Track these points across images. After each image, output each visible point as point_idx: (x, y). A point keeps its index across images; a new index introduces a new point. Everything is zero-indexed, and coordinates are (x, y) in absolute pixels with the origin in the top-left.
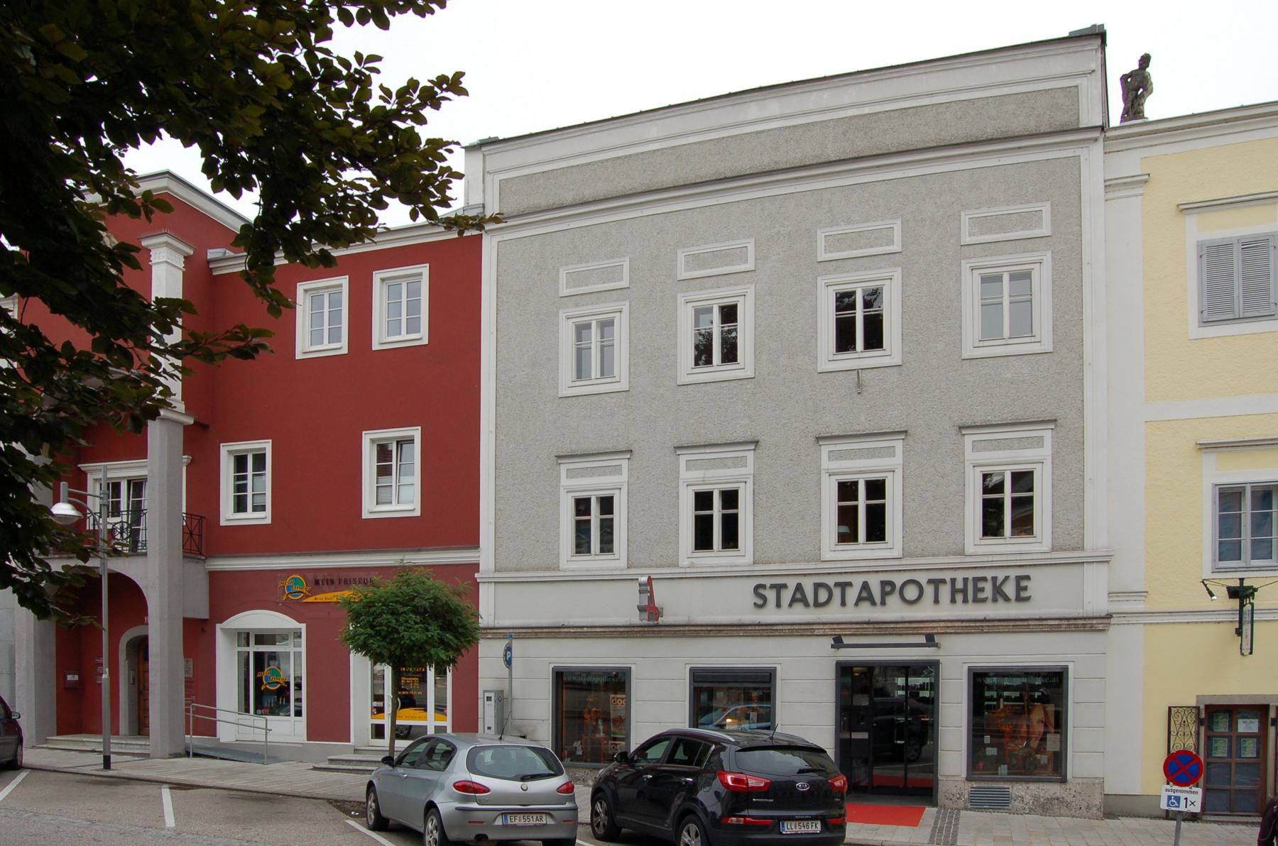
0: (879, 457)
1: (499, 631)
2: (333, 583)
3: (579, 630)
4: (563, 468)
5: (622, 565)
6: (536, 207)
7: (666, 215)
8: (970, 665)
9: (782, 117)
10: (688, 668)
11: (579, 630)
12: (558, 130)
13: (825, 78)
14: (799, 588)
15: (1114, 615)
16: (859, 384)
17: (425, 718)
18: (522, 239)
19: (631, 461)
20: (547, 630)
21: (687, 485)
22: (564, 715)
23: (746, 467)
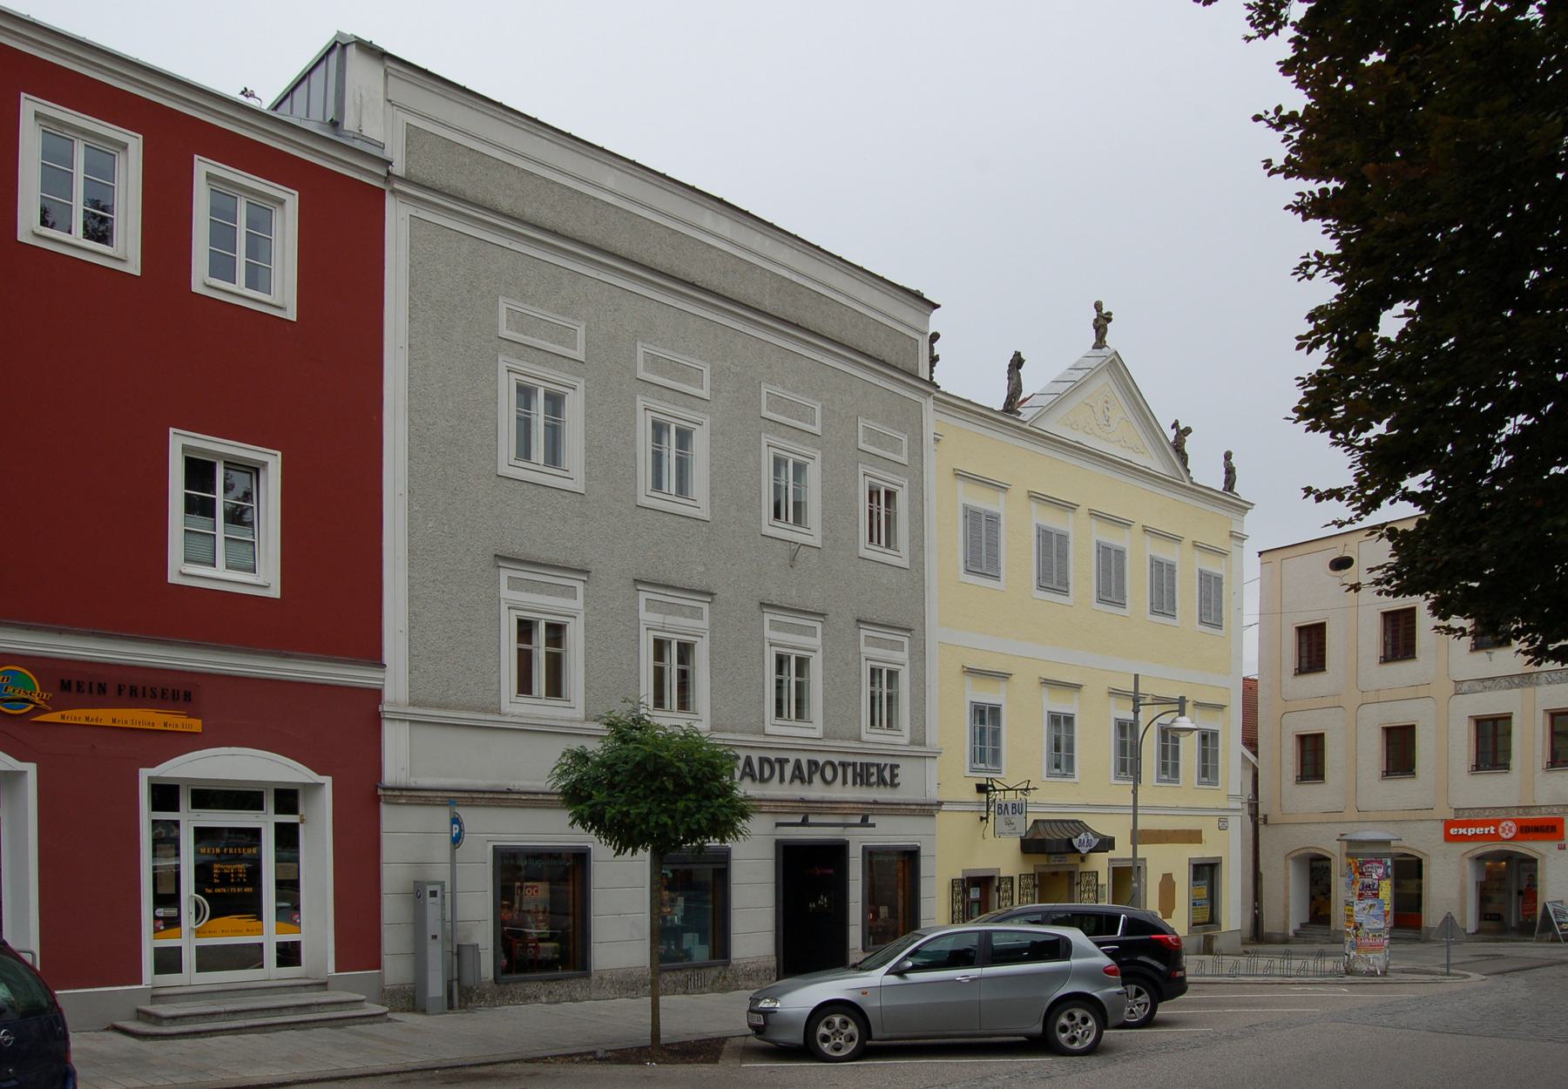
1: (421, 794)
2: (104, 692)
3: (532, 797)
5: (578, 716)
7: (624, 292)
9: (731, 242)
10: (490, 848)
11: (532, 797)
12: (500, 105)
13: (464, 89)
14: (798, 764)
17: (260, 932)
19: (712, 605)
20: (491, 796)
22: (710, 906)
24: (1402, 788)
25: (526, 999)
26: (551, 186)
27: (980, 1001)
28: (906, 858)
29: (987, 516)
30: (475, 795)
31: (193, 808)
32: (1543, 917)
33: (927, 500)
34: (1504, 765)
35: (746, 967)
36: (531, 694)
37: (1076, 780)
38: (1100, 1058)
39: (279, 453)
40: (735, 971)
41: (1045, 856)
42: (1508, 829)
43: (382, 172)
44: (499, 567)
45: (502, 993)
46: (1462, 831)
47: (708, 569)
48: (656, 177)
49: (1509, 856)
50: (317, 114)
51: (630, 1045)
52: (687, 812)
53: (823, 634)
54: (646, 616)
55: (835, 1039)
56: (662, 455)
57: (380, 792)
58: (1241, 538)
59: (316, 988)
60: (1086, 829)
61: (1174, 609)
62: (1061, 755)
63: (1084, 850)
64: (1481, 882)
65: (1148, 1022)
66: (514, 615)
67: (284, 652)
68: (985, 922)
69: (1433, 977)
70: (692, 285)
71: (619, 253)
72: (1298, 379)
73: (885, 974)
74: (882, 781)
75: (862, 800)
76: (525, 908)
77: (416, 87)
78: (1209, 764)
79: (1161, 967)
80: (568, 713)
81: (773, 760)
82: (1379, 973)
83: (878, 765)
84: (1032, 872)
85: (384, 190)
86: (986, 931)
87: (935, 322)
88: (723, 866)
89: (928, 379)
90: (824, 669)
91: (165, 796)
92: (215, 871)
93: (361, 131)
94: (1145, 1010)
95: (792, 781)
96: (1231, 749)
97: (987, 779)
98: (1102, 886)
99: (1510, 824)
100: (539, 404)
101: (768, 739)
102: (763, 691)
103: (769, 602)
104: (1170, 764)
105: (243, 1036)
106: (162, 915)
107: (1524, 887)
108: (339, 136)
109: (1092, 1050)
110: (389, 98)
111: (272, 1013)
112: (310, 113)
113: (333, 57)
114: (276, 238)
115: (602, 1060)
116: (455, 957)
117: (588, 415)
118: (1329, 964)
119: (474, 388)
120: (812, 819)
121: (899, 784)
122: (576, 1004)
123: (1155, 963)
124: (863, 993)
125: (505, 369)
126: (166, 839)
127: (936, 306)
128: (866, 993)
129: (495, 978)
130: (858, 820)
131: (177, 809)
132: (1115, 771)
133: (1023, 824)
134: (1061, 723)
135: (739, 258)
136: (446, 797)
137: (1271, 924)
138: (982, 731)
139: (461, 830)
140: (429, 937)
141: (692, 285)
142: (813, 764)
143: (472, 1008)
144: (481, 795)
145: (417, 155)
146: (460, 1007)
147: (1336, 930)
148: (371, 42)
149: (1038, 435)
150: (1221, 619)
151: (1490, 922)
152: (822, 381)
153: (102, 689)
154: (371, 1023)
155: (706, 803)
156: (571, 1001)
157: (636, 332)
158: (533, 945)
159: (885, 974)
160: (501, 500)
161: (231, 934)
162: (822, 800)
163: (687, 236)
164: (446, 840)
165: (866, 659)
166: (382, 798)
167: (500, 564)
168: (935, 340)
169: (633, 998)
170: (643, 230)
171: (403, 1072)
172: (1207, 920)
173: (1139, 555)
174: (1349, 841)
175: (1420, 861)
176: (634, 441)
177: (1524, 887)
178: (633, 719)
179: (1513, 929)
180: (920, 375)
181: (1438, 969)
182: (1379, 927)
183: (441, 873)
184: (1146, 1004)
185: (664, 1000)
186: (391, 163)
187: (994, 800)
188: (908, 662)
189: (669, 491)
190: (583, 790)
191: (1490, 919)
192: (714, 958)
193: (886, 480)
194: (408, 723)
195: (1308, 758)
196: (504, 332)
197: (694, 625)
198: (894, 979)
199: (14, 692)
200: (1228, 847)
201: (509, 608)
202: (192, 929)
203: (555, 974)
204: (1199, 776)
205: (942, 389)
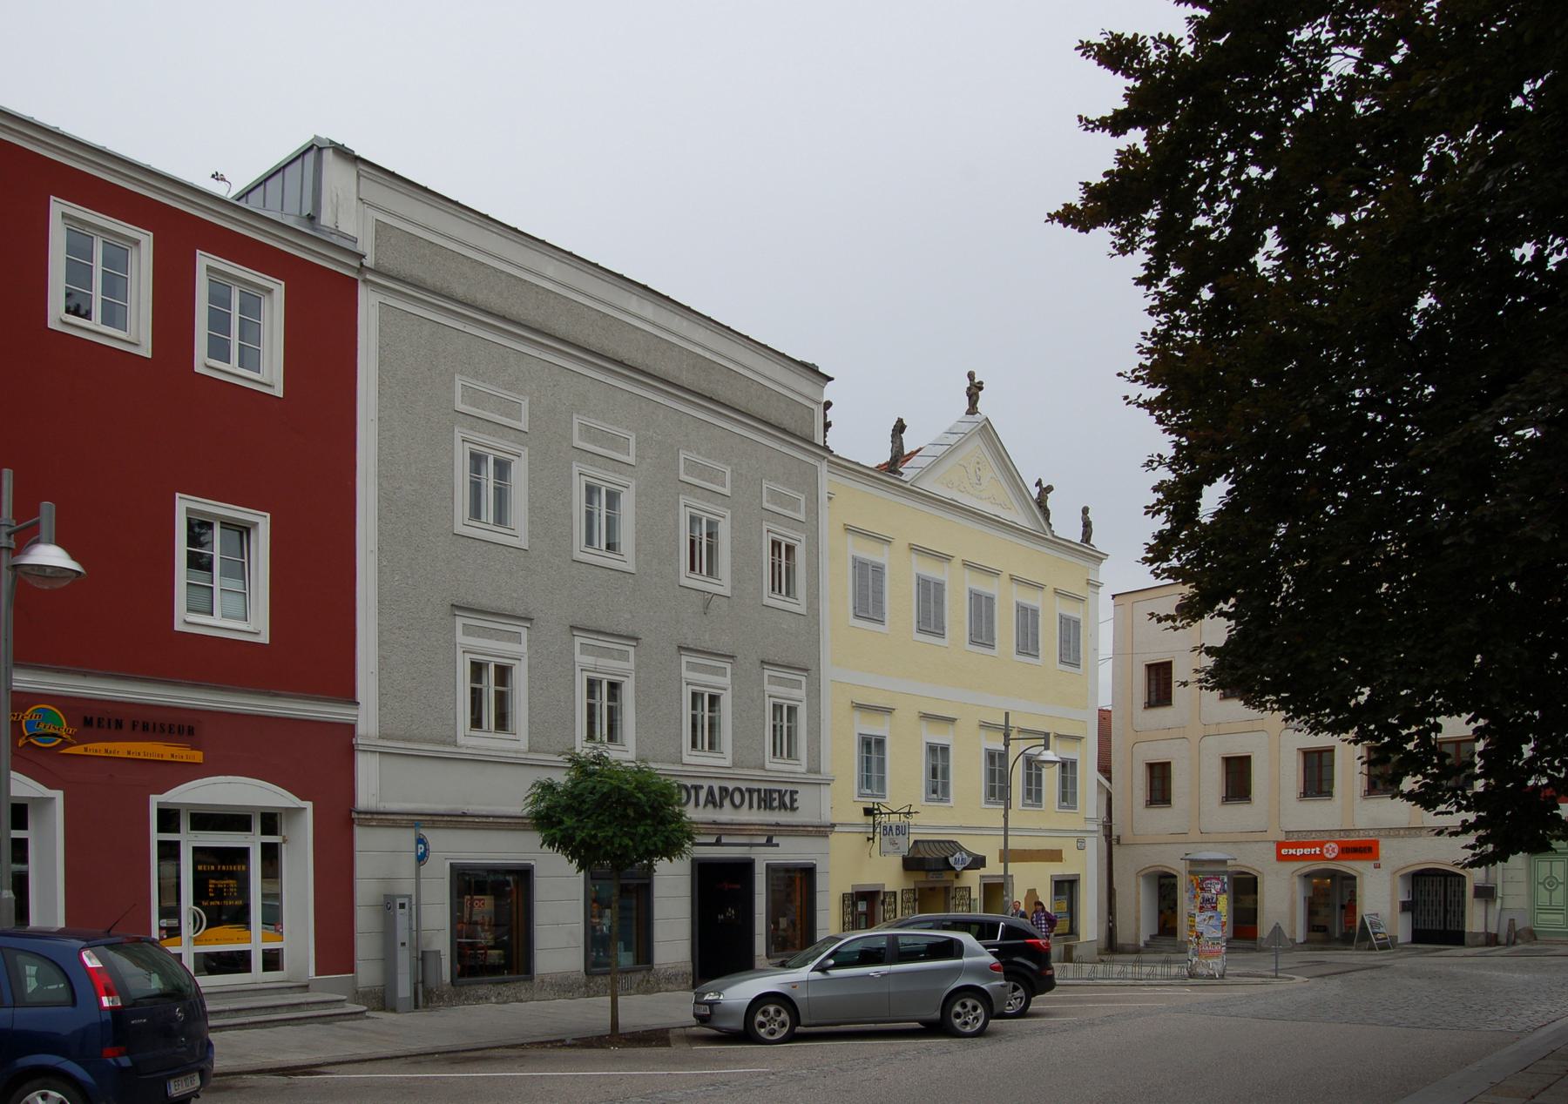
2: (121, 727)
3: (484, 820)
6: (421, 282)
8: (452, 861)
9: (653, 324)
10: (448, 866)
11: (484, 820)
12: (456, 203)
13: (425, 189)
14: (711, 789)
17: (249, 940)
18: (409, 315)
20: (449, 819)
21: (464, 652)
22: (634, 914)
24: (1238, 813)
25: (479, 999)
26: (498, 274)
27: (889, 993)
28: (804, 874)
29: (873, 567)
30: (436, 818)
31: (191, 830)
32: (1361, 928)
33: (822, 552)
34: (1329, 792)
36: (481, 728)
37: (951, 804)
38: (988, 1039)
42: (1332, 850)
43: (356, 264)
44: (455, 615)
46: (1292, 851)
47: (633, 617)
48: (589, 266)
49: (1333, 874)
50: (292, 206)
52: (645, 836)
53: (732, 674)
54: (581, 659)
57: (354, 815)
58: (1097, 586)
59: (300, 989)
60: (961, 849)
61: (1038, 650)
62: (938, 780)
63: (959, 868)
64: (1309, 898)
65: (1022, 1013)
67: (272, 691)
69: (1264, 979)
72: (1145, 544)
73: (811, 971)
74: (783, 806)
75: (766, 823)
76: (475, 918)
78: (1069, 790)
79: (1034, 967)
80: (514, 745)
82: (1217, 976)
83: (779, 791)
84: (913, 887)
85: (357, 280)
86: (893, 935)
87: (829, 392)
88: (647, 881)
89: (822, 445)
90: (733, 706)
91: (169, 819)
92: (210, 886)
94: (1020, 1003)
96: (1088, 775)
97: (874, 803)
98: (974, 900)
99: (1333, 845)
101: (685, 768)
103: (685, 646)
104: (1034, 791)
106: (165, 925)
107: (1346, 902)
109: (980, 1033)
110: (361, 197)
112: (285, 207)
113: (310, 157)
115: (570, 1046)
116: (420, 962)
118: (1175, 970)
120: (724, 840)
121: (798, 808)
123: (1029, 963)
126: (170, 852)
127: (830, 379)
129: (452, 981)
130: (763, 840)
131: (178, 831)
132: (986, 797)
133: (905, 845)
134: (938, 753)
135: (661, 338)
137: (1123, 937)
138: (868, 760)
139: (426, 850)
142: (723, 790)
143: (434, 1007)
144: (440, 818)
146: (424, 1007)
147: (1182, 941)
148: (343, 145)
149: (919, 493)
150: (1079, 659)
151: (1319, 934)
152: (732, 447)
153: (119, 724)
155: (660, 827)
156: (516, 1001)
157: (573, 405)
158: (482, 951)
159: (811, 971)
160: (457, 555)
161: (224, 942)
162: (731, 822)
165: (770, 696)
166: (356, 821)
167: (457, 613)
168: (828, 408)
171: (410, 1056)
172: (1067, 931)
173: (1006, 601)
174: (1192, 861)
175: (1256, 878)
176: (570, 503)
177: (1346, 902)
179: (1337, 939)
180: (816, 442)
181: (1269, 973)
182: (1217, 936)
183: (407, 887)
184: (1021, 998)
186: (364, 257)
187: (880, 822)
188: (526, 656)
190: (554, 816)
191: (1317, 931)
193: (787, 535)
194: (378, 754)
195: (1157, 783)
196: (460, 406)
197: (622, 666)
198: (818, 975)
199: (45, 727)
200: (1085, 864)
201: (464, 652)
202: (191, 937)
203: (501, 977)
204: (927, 793)
205: (835, 453)
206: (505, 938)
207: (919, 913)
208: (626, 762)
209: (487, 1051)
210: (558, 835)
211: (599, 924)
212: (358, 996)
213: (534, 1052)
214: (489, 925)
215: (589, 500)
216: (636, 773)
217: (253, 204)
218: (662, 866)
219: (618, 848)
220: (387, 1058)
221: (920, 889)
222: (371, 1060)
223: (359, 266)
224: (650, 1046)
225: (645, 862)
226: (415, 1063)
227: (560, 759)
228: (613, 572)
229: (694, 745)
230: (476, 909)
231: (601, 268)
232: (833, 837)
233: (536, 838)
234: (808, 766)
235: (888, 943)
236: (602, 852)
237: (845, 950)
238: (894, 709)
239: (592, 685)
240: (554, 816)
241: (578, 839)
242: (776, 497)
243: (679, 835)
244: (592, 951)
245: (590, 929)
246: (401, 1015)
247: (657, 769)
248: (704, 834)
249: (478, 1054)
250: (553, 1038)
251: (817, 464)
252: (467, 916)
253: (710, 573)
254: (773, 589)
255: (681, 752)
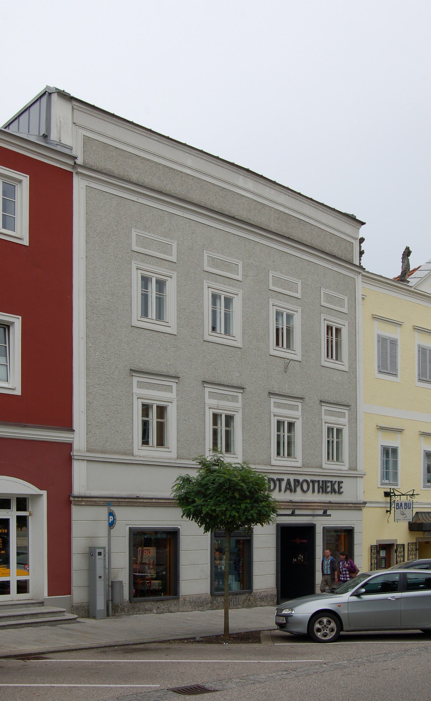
0: (292, 410)
1: (93, 499)
3: (150, 501)
4: (207, 390)
9: (253, 193)
10: (127, 529)
11: (150, 501)
12: (132, 123)
13: (113, 115)
14: (289, 482)
15: (367, 503)
16: (286, 368)
19: (244, 394)
20: (128, 500)
23: (238, 402)
25: (146, 611)
26: (158, 166)
28: (346, 534)
35: (260, 594)
36: (148, 445)
39: (20, 317)
40: (255, 596)
41: (422, 532)
43: (72, 163)
44: (133, 376)
45: (133, 608)
50: (34, 130)
51: (211, 634)
53: (302, 409)
54: (209, 401)
55: (324, 630)
56: (148, 296)
57: (72, 499)
66: (140, 401)
68: (404, 568)
70: (233, 218)
71: (194, 202)
73: (351, 596)
74: (333, 491)
75: (322, 501)
76: (144, 561)
77: (107, 123)
80: (168, 455)
81: (275, 479)
83: (331, 482)
85: (72, 173)
86: (403, 573)
87: (363, 232)
88: (249, 538)
89: (359, 265)
93: (60, 140)
95: (285, 491)
97: (390, 489)
100: (153, 286)
101: (273, 468)
102: (270, 441)
105: (6, 630)
108: (48, 143)
110: (74, 122)
111: (19, 618)
113: (44, 99)
114: (18, 200)
115: (199, 642)
116: (110, 588)
117: (178, 292)
119: (119, 279)
120: (297, 512)
121: (343, 492)
122: (172, 614)
124: (339, 606)
125: (135, 268)
127: (363, 224)
128: (340, 606)
129: (130, 599)
130: (321, 512)
133: (410, 515)
135: (257, 201)
136: (104, 501)
138: (387, 462)
139: (114, 519)
140: (98, 577)
141: (233, 218)
142: (297, 481)
143: (119, 616)
144: (123, 500)
145: (89, 153)
146: (113, 616)
148: (64, 91)
149: (419, 294)
154: (69, 623)
155: (255, 505)
156: (169, 612)
159: (351, 596)
160: (133, 339)
162: (301, 501)
163: (230, 191)
164: (105, 525)
166: (73, 502)
169: (202, 611)
170: (207, 189)
171: (100, 647)
178: (215, 460)
180: (354, 263)
183: (102, 542)
185: (231, 612)
186: (76, 158)
187: (394, 501)
188: (175, 400)
189: (152, 318)
192: (243, 589)
194: (86, 461)
198: (355, 598)
201: (138, 398)
204: (424, 482)
206: (164, 573)
207: (419, 558)
208: (235, 464)
209: (147, 644)
210: (192, 510)
211: (220, 564)
212: (74, 609)
213: (175, 646)
214: (153, 565)
215: (214, 303)
216: (240, 471)
217: (12, 130)
218: (257, 529)
219: (229, 518)
220: (85, 649)
221: (419, 542)
222: (76, 650)
223: (74, 165)
224: (248, 643)
225: (246, 526)
226: (102, 652)
227: (194, 462)
228: (228, 348)
229: (278, 454)
230: (145, 555)
231: (221, 159)
232: (364, 510)
233: (179, 511)
234: (349, 466)
235: (400, 578)
236: (219, 520)
237: (372, 582)
238: (404, 430)
239: (216, 417)
240: (190, 498)
241: (204, 512)
242: (330, 299)
243: (267, 509)
244: (215, 581)
245: (214, 567)
246: (99, 620)
247: (253, 469)
248: (283, 509)
249: (142, 646)
250: (188, 637)
251: (355, 277)
252: (139, 560)
253: (288, 347)
254: (328, 356)
255: (270, 458)
